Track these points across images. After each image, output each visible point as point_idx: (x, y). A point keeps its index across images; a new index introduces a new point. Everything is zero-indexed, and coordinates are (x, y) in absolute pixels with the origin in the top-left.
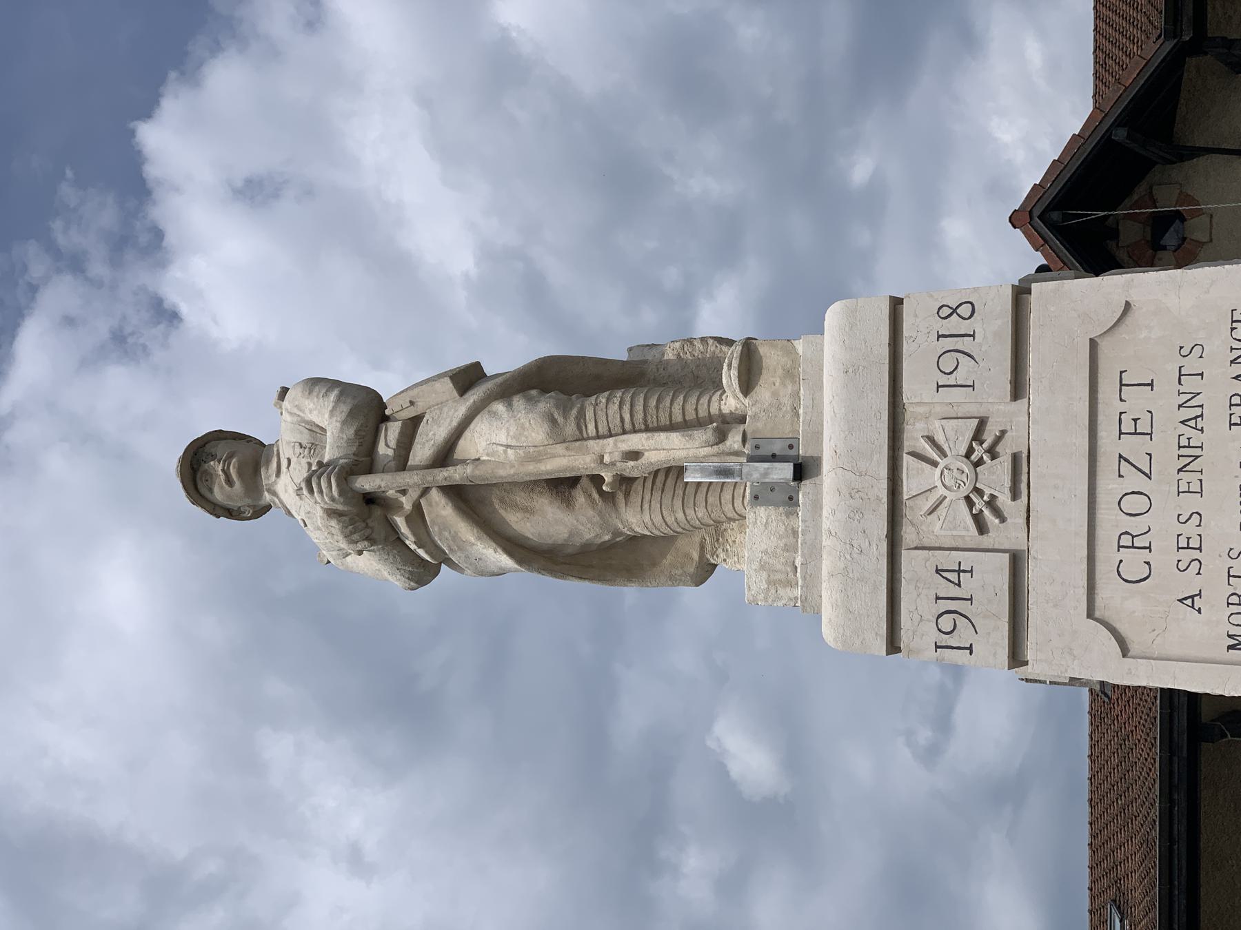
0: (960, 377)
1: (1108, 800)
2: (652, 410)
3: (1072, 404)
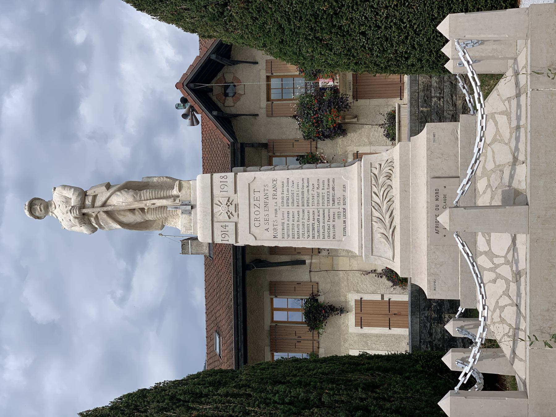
0: (225, 190)
1: (213, 296)
2: (156, 194)
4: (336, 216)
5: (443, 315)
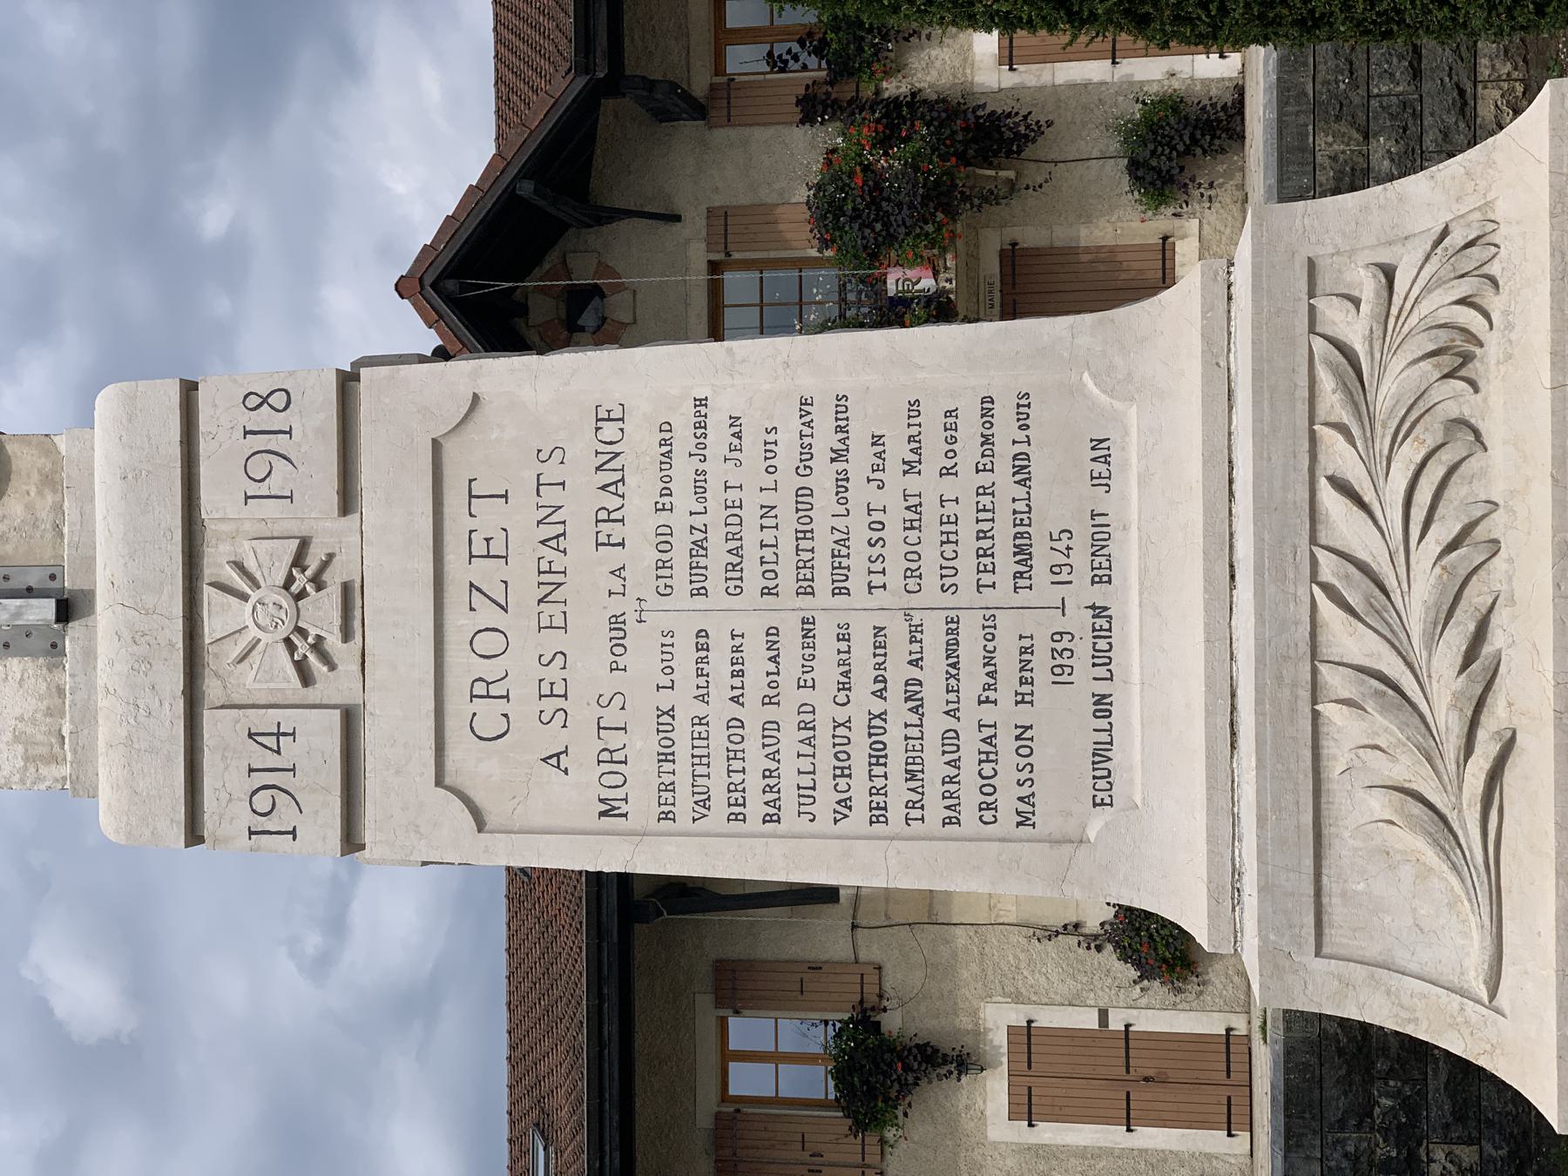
0: (274, 485)
3: (413, 520)
4: (1041, 662)
5: (1422, 1152)
